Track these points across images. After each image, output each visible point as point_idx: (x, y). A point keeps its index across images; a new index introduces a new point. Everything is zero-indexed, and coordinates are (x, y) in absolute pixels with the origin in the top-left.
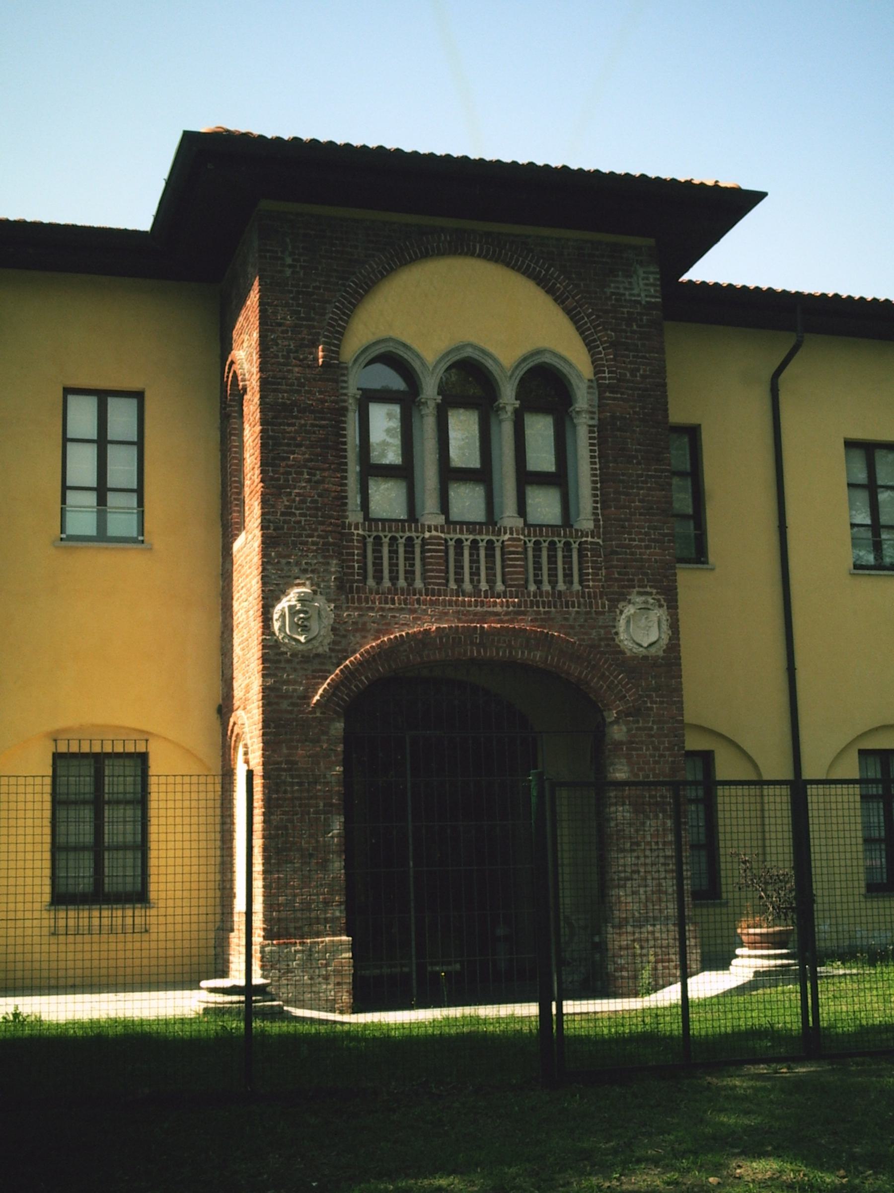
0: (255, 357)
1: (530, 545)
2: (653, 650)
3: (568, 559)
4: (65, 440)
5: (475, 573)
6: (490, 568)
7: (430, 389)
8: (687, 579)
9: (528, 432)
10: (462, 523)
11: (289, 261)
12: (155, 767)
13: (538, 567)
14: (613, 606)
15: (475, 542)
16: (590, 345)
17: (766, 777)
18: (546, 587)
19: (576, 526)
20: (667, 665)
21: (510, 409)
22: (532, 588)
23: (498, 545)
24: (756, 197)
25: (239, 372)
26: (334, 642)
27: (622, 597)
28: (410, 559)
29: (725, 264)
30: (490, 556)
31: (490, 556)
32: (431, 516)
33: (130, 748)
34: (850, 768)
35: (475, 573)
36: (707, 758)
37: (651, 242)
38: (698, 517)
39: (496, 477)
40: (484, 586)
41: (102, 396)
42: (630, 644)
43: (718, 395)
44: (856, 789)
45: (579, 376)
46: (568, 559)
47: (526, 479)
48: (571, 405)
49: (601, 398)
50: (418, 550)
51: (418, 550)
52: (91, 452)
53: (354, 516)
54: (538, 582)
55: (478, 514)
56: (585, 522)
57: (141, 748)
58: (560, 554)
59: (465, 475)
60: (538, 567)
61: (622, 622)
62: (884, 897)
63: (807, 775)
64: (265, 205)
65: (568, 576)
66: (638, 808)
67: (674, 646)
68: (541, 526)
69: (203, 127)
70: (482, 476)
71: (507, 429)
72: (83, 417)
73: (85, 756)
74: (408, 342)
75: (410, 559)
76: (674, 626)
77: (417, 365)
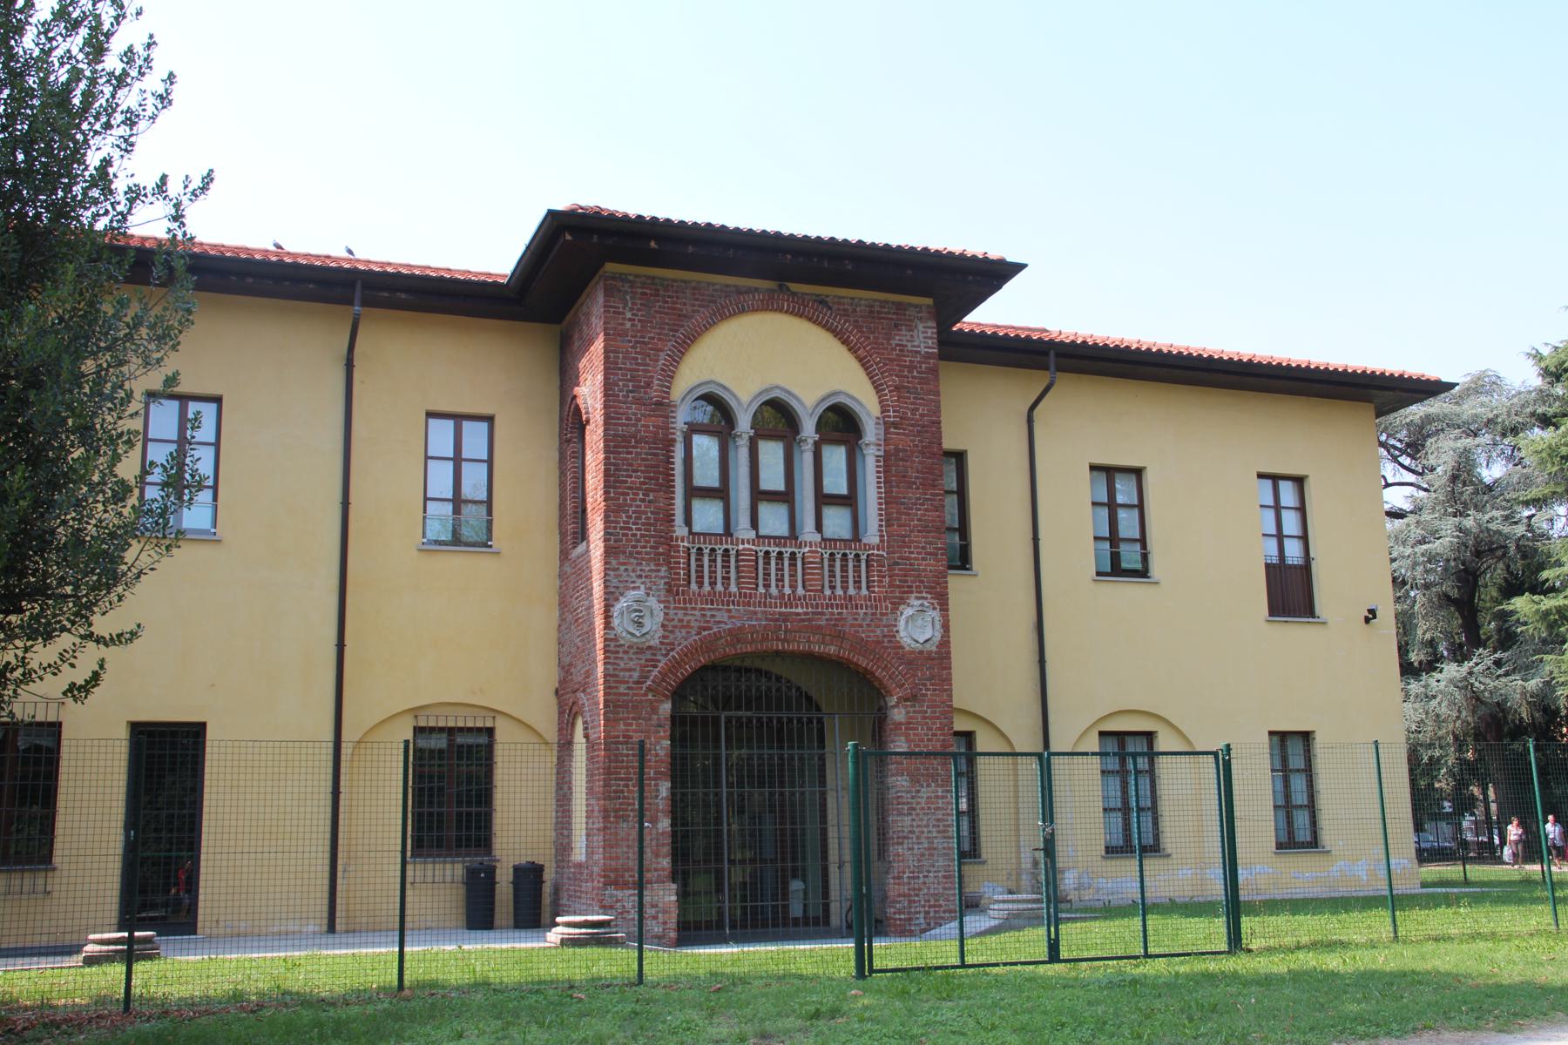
0: (599, 395)
1: (826, 556)
2: (928, 645)
3: (857, 569)
4: (427, 458)
5: (780, 580)
6: (793, 575)
7: (744, 423)
8: (956, 583)
9: (825, 460)
10: (769, 537)
11: (629, 315)
12: (498, 736)
13: (832, 575)
14: (894, 609)
15: (780, 553)
16: (878, 388)
17: (1018, 750)
18: (839, 592)
19: (865, 541)
20: (939, 659)
21: (810, 441)
22: (828, 592)
23: (799, 556)
24: (1013, 269)
25: (582, 407)
26: (664, 637)
27: (902, 601)
28: (726, 567)
29: (993, 313)
30: (793, 565)
31: (793, 565)
32: (743, 530)
33: (479, 724)
34: (1093, 744)
35: (780, 580)
36: (968, 736)
37: (929, 301)
38: (963, 529)
39: (797, 497)
40: (787, 591)
41: (458, 418)
42: (909, 641)
43: (982, 419)
44: (1097, 759)
45: (868, 414)
46: (857, 569)
47: (823, 500)
48: (860, 437)
49: (887, 432)
50: (733, 560)
51: (733, 560)
52: (467, 491)
53: (680, 530)
54: (833, 588)
55: (782, 529)
56: (872, 536)
57: (489, 724)
58: (851, 564)
59: (773, 497)
60: (832, 575)
61: (902, 623)
62: (23, 871)
63: (1054, 748)
64: (610, 267)
65: (857, 582)
66: (915, 779)
67: (945, 643)
68: (835, 540)
69: (561, 206)
70: (786, 497)
71: (808, 458)
72: (441, 435)
73: (441, 729)
74: (727, 384)
75: (726, 567)
76: (946, 627)
77: (733, 403)
